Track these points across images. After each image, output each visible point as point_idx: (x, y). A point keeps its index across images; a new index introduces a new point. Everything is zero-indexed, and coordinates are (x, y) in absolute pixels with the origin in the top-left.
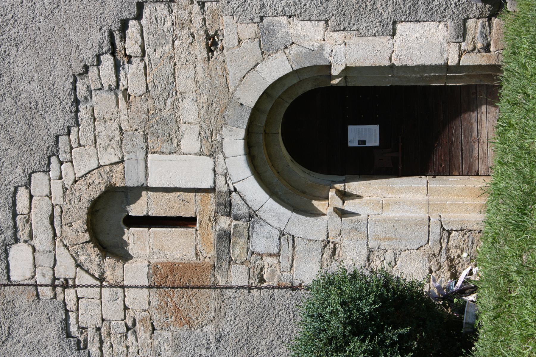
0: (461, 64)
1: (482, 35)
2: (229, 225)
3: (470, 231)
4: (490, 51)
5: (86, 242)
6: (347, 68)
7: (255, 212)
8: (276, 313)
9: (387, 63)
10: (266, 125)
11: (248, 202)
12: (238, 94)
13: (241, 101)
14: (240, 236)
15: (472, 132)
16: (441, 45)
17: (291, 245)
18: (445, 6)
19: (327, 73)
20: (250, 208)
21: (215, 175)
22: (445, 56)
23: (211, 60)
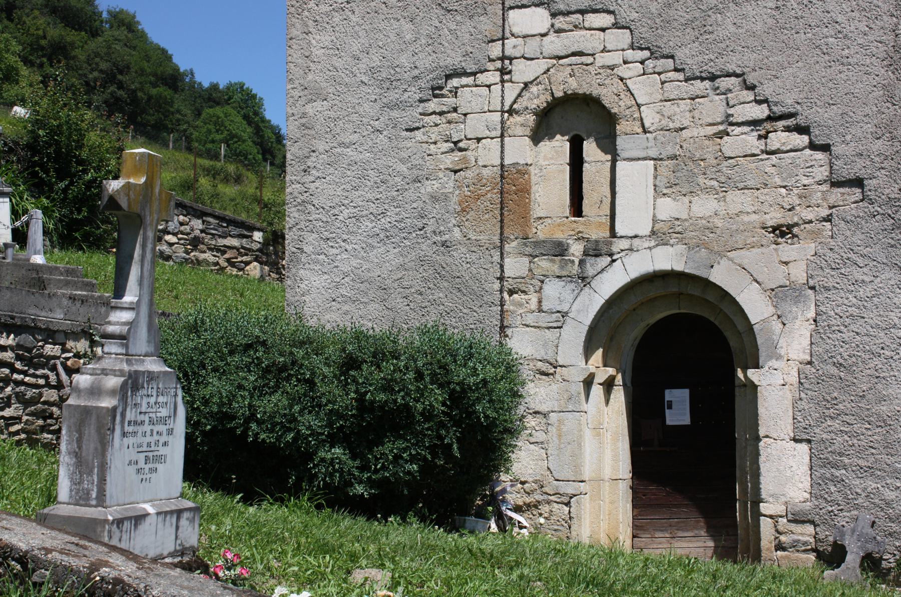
0: (762, 518)
1: (795, 541)
3: (570, 527)
4: (776, 551)
5: (552, 94)
8: (475, 308)
11: (600, 275)
12: (724, 262)
13: (716, 265)
14: (562, 268)
15: (683, 530)
16: (783, 495)
18: (829, 499)
20: (593, 278)
21: (631, 237)
22: (771, 500)
23: (763, 231)
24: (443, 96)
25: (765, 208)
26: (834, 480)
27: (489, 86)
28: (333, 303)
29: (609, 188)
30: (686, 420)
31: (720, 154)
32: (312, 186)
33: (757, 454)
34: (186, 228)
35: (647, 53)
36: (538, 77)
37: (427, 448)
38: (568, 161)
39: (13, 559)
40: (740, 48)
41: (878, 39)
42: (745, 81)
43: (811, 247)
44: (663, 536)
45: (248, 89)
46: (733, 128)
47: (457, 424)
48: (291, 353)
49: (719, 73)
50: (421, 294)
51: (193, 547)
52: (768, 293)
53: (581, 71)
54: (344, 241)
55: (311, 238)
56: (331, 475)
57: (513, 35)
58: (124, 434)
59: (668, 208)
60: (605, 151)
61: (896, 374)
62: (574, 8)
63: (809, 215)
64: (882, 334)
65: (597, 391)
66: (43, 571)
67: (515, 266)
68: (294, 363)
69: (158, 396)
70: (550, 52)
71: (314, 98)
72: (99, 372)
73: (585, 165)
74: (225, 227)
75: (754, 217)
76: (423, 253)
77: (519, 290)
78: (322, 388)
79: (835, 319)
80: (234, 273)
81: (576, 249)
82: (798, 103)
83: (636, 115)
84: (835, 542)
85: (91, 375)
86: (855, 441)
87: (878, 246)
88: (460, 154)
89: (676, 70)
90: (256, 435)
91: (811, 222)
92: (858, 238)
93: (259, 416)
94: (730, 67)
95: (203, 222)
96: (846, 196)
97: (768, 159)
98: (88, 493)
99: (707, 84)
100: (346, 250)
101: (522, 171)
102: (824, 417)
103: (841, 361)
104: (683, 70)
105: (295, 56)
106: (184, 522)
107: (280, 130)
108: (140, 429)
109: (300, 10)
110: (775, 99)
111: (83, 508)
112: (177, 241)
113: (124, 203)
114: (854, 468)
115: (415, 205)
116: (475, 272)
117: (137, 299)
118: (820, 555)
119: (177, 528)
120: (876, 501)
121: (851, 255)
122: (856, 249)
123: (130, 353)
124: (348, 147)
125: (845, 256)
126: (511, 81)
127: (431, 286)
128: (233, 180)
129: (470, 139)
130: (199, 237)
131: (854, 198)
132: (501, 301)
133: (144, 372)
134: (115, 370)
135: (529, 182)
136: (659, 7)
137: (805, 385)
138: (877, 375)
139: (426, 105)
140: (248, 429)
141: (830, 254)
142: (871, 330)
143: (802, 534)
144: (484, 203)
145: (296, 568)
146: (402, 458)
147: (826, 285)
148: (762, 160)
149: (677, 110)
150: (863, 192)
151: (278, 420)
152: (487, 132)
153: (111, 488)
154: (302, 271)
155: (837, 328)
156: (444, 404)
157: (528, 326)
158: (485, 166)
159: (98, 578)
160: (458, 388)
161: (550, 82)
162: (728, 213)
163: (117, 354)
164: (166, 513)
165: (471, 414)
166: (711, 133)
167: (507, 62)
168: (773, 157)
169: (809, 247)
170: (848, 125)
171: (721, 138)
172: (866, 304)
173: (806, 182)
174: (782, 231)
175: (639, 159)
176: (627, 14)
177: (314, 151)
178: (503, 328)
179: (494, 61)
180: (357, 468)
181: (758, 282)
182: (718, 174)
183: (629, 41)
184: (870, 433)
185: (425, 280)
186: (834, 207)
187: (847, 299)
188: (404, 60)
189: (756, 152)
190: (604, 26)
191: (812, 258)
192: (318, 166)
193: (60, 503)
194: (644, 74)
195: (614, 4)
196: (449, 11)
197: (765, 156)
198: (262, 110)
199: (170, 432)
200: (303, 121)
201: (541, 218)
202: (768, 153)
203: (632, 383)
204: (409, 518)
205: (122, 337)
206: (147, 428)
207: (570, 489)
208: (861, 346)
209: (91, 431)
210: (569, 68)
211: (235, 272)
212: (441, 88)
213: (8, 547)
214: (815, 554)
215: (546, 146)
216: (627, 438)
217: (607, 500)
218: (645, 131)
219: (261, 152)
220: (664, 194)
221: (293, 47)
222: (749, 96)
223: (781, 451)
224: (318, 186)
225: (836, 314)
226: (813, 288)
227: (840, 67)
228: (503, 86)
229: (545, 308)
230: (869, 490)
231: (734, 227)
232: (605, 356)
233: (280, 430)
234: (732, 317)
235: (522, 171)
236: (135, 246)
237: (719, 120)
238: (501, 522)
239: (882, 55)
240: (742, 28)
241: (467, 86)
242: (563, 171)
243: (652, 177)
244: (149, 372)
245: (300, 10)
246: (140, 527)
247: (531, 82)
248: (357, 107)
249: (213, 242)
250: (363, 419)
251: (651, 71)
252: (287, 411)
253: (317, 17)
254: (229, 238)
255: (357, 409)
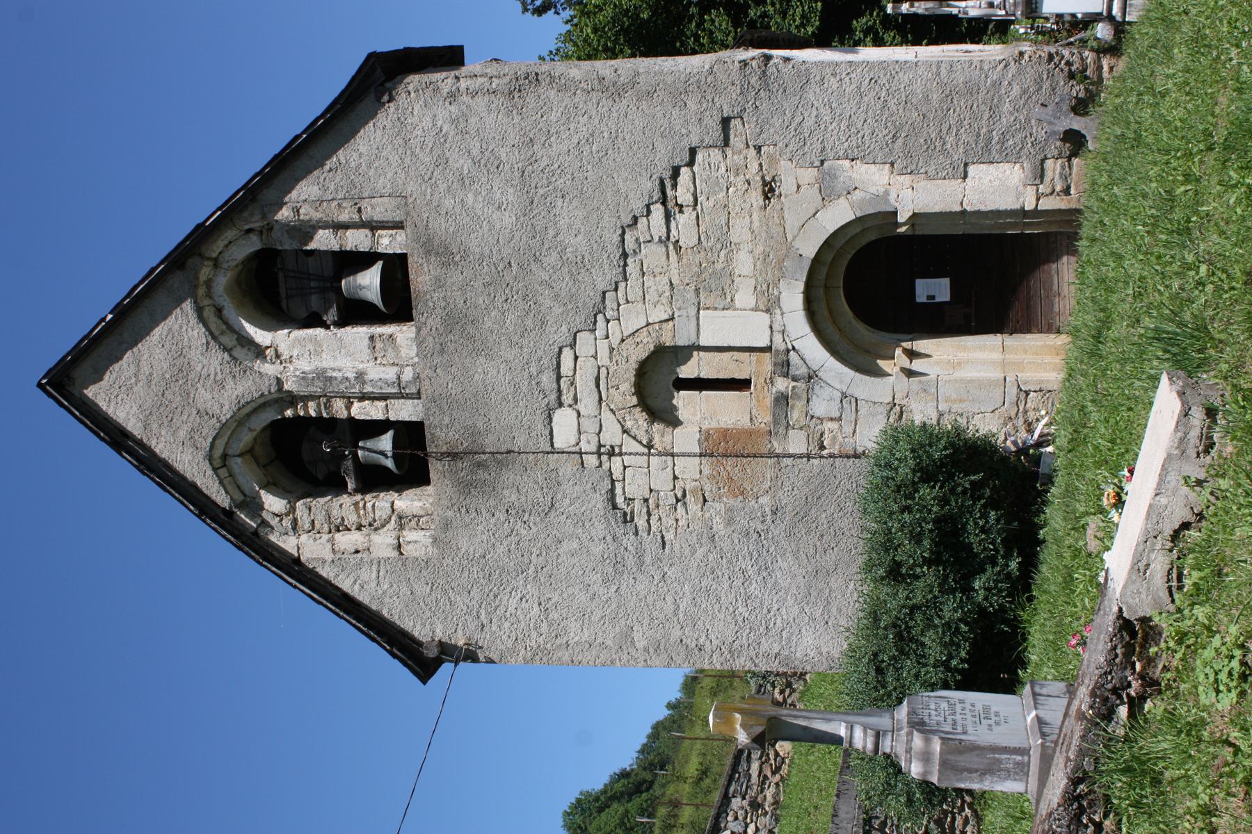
0: (1039, 208)
1: (1061, 177)
2: (787, 387)
3: (1050, 391)
4: (1070, 194)
5: (634, 406)
6: (915, 215)
7: (815, 372)
8: (837, 483)
9: (958, 209)
10: (826, 279)
11: (807, 361)
12: (796, 244)
13: (800, 252)
14: (799, 398)
15: (1052, 285)
16: (1017, 189)
17: (854, 408)
18: (1020, 146)
19: (893, 221)
20: (809, 368)
21: (772, 332)
22: (1021, 200)
23: (768, 208)
24: (632, 512)
25: (747, 206)
26: (1002, 142)
27: (625, 467)
28: (829, 623)
29: (724, 354)
30: (946, 282)
31: (695, 249)
32: (715, 642)
33: (978, 213)
34: (741, 814)
35: (600, 317)
36: (618, 420)
37: (974, 503)
38: (698, 392)
39: (1075, 791)
40: (598, 230)
41: (595, 106)
42: (629, 226)
43: (784, 164)
44: (1057, 304)
45: (570, 807)
46: (671, 236)
47: (951, 476)
48: (885, 628)
49: (621, 250)
50: (822, 536)
51: (1067, 686)
52: (826, 203)
53: (613, 379)
54: (769, 611)
55: (765, 646)
56: (1000, 591)
57: (578, 444)
58: (965, 733)
59: (745, 297)
60: (689, 357)
61: (903, 86)
62: (555, 385)
63: (754, 167)
64: (866, 99)
65: (917, 365)
66: (1085, 763)
67: (797, 443)
68: (895, 626)
69: (929, 709)
70: (594, 408)
71: (630, 640)
72: (909, 755)
73: (702, 376)
74: (739, 776)
75: (755, 217)
76: (783, 534)
77: (820, 439)
78: (918, 599)
79: (851, 142)
80: (787, 767)
81: (782, 384)
82: (651, 177)
83: (657, 327)
84: (1062, 140)
85: (911, 763)
86: (966, 122)
87: (785, 104)
88: (688, 496)
89: (616, 289)
90: (963, 661)
91: (761, 165)
92: (777, 122)
93: (944, 658)
94: (615, 239)
95: (734, 797)
96: (738, 133)
97: (701, 204)
98: (1018, 764)
99: (629, 261)
100: (778, 610)
101: (706, 436)
102: (944, 150)
103: (891, 135)
104: (616, 283)
105: (589, 658)
106: (1044, 691)
107: (615, 774)
108: (959, 722)
109: (545, 652)
110: (647, 198)
111: (1031, 768)
112: (753, 824)
113: (759, 729)
114: (991, 123)
115: (736, 541)
116: (801, 482)
117: (843, 723)
118: (1074, 154)
119: (1049, 696)
120: (1022, 102)
121: (792, 127)
122: (786, 123)
123: (891, 729)
124: (679, 607)
125: (793, 133)
126: (621, 446)
127: (814, 525)
128: (676, 810)
129: (675, 486)
130: (750, 801)
131: (740, 126)
132: (830, 457)
133: (908, 718)
134: (907, 740)
135: (717, 430)
136: (557, 306)
137: (913, 169)
138: (904, 103)
139: (640, 528)
140: (956, 670)
141: (791, 147)
142: (862, 109)
143: (1054, 171)
144: (737, 473)
145: (1086, 600)
146: (983, 526)
147: (819, 150)
148: (702, 209)
149: (654, 288)
150: (734, 118)
151: (947, 639)
152: (668, 469)
153: (1014, 743)
154: (798, 655)
155: (860, 140)
156: (934, 487)
157: (855, 432)
158: (701, 472)
159: (1091, 712)
160: (919, 474)
161: (623, 409)
162: (751, 241)
163: (893, 741)
164: (1035, 703)
165: (942, 464)
166: (675, 256)
167: (603, 450)
168: (699, 199)
169: (784, 166)
170: (672, 132)
171: (680, 248)
172: (838, 114)
173: (724, 169)
174: (769, 191)
175: (698, 324)
176: (563, 335)
177: (681, 641)
178: (856, 456)
179: (601, 462)
180: (993, 567)
181: (816, 213)
182: (714, 250)
183: (587, 333)
184: (958, 109)
185: (808, 532)
186: (747, 143)
187: (833, 131)
188: (597, 549)
189: (695, 215)
190: (573, 357)
191: (794, 163)
192: (696, 636)
193: (1026, 790)
194: (619, 320)
195: (553, 347)
196: (552, 505)
197: (699, 207)
198: (593, 792)
199: (962, 701)
200: (651, 650)
201: (751, 419)
202: (696, 204)
203: (910, 333)
204: (1041, 521)
205: (877, 735)
206: (958, 717)
207: (1012, 392)
208: (877, 118)
209: (963, 760)
210: (610, 390)
211: (785, 768)
212: (625, 514)
213: (1064, 796)
214: (1073, 159)
215: (682, 414)
216: (963, 338)
217: (1024, 356)
218: (672, 319)
219: (639, 795)
220: (732, 300)
221: (580, 659)
222: (643, 222)
223: (975, 190)
224: (715, 637)
225: (847, 141)
226: (822, 162)
227: (619, 139)
228: (626, 453)
229: (837, 415)
230: (1011, 109)
231: (764, 235)
232: (884, 358)
233: (957, 638)
234: (849, 237)
235: (706, 436)
236: (796, 725)
237: (664, 249)
238: (1044, 445)
239: (610, 102)
240: (580, 229)
241: (624, 489)
242: (707, 397)
243: (715, 312)
244: (909, 713)
245: (545, 652)
246: (1048, 721)
247: (623, 427)
248: (639, 597)
249: (755, 787)
250: (948, 561)
251: (616, 313)
252: (940, 630)
253: (553, 635)
254: (751, 772)
255: (937, 566)
